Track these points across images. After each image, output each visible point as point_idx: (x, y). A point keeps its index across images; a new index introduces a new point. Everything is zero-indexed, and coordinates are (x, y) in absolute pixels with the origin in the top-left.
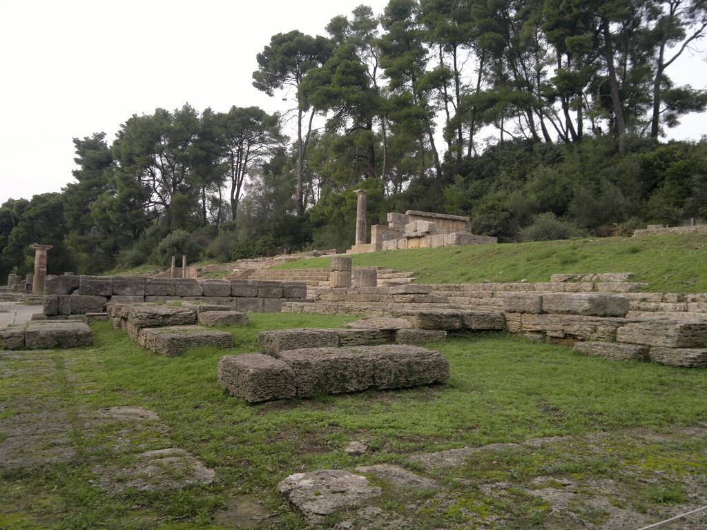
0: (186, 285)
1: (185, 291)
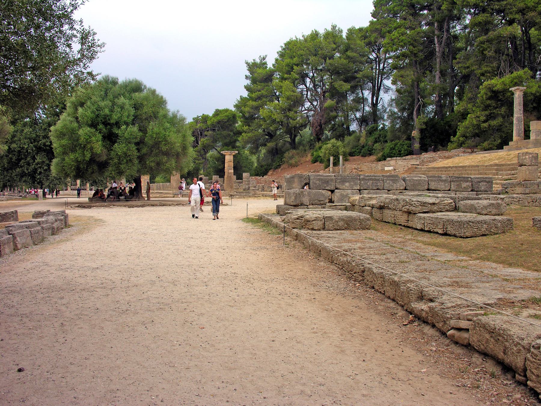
0: (392, 180)
1: (392, 186)
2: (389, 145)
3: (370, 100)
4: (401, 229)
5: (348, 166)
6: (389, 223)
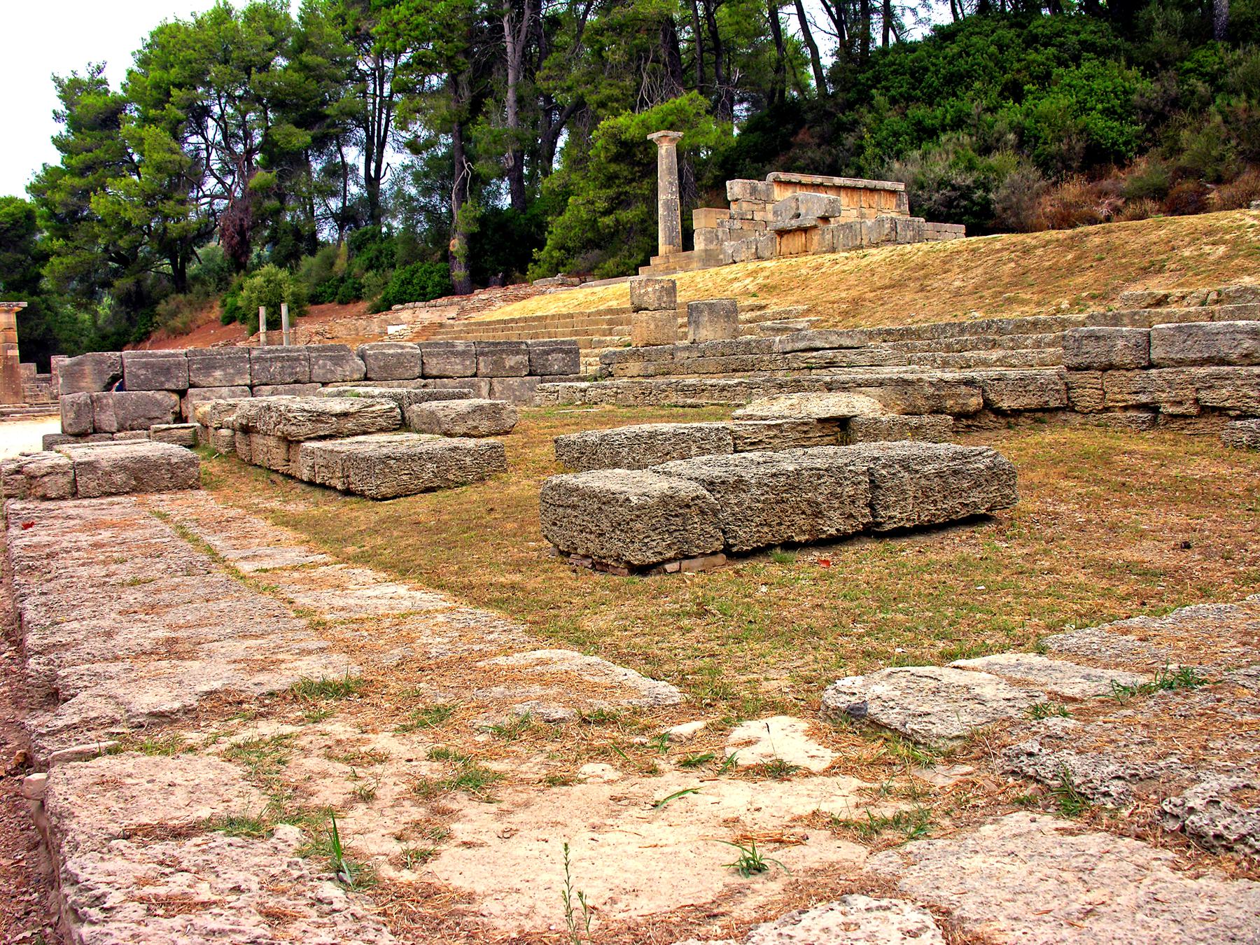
0: (331, 358)
1: (332, 372)
2: (396, 275)
3: (362, 172)
4: (273, 482)
5: (305, 327)
6: (260, 467)
